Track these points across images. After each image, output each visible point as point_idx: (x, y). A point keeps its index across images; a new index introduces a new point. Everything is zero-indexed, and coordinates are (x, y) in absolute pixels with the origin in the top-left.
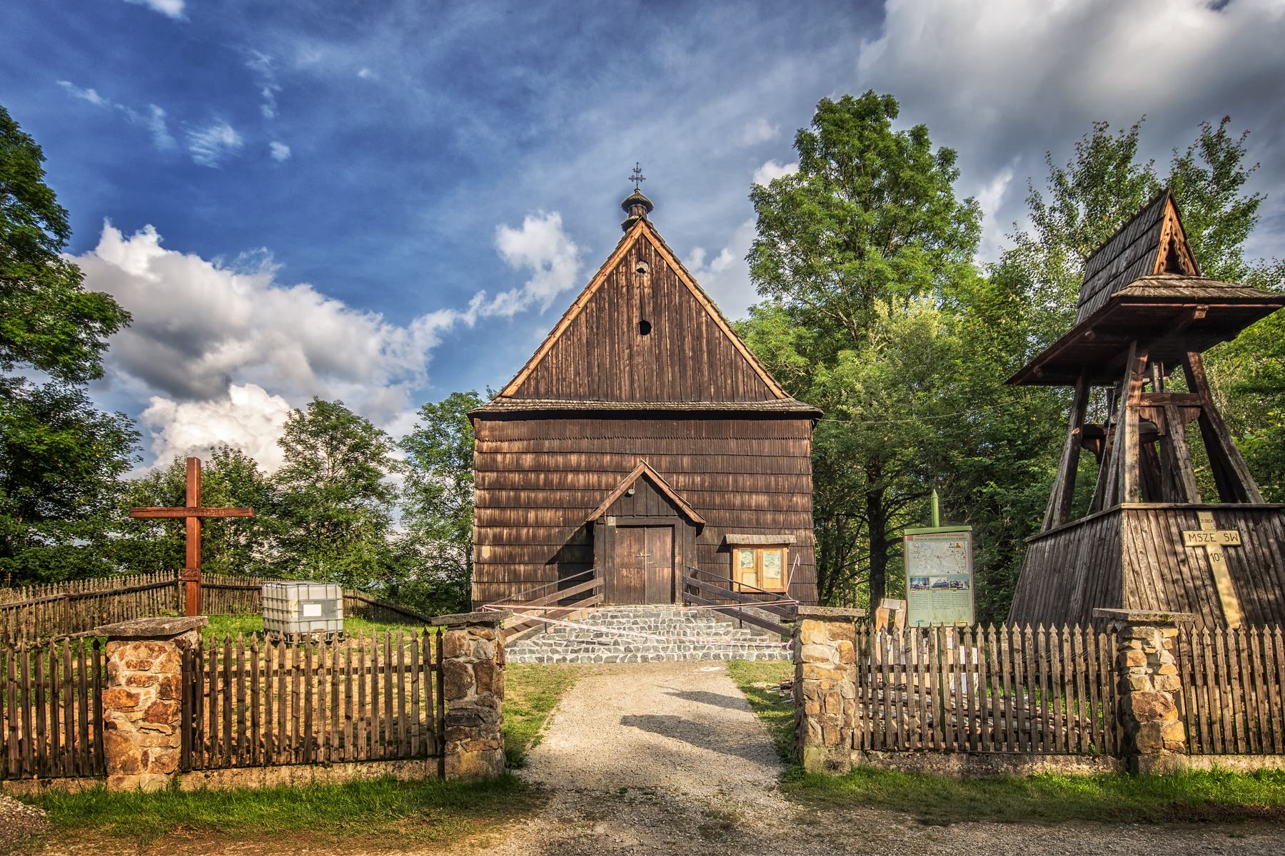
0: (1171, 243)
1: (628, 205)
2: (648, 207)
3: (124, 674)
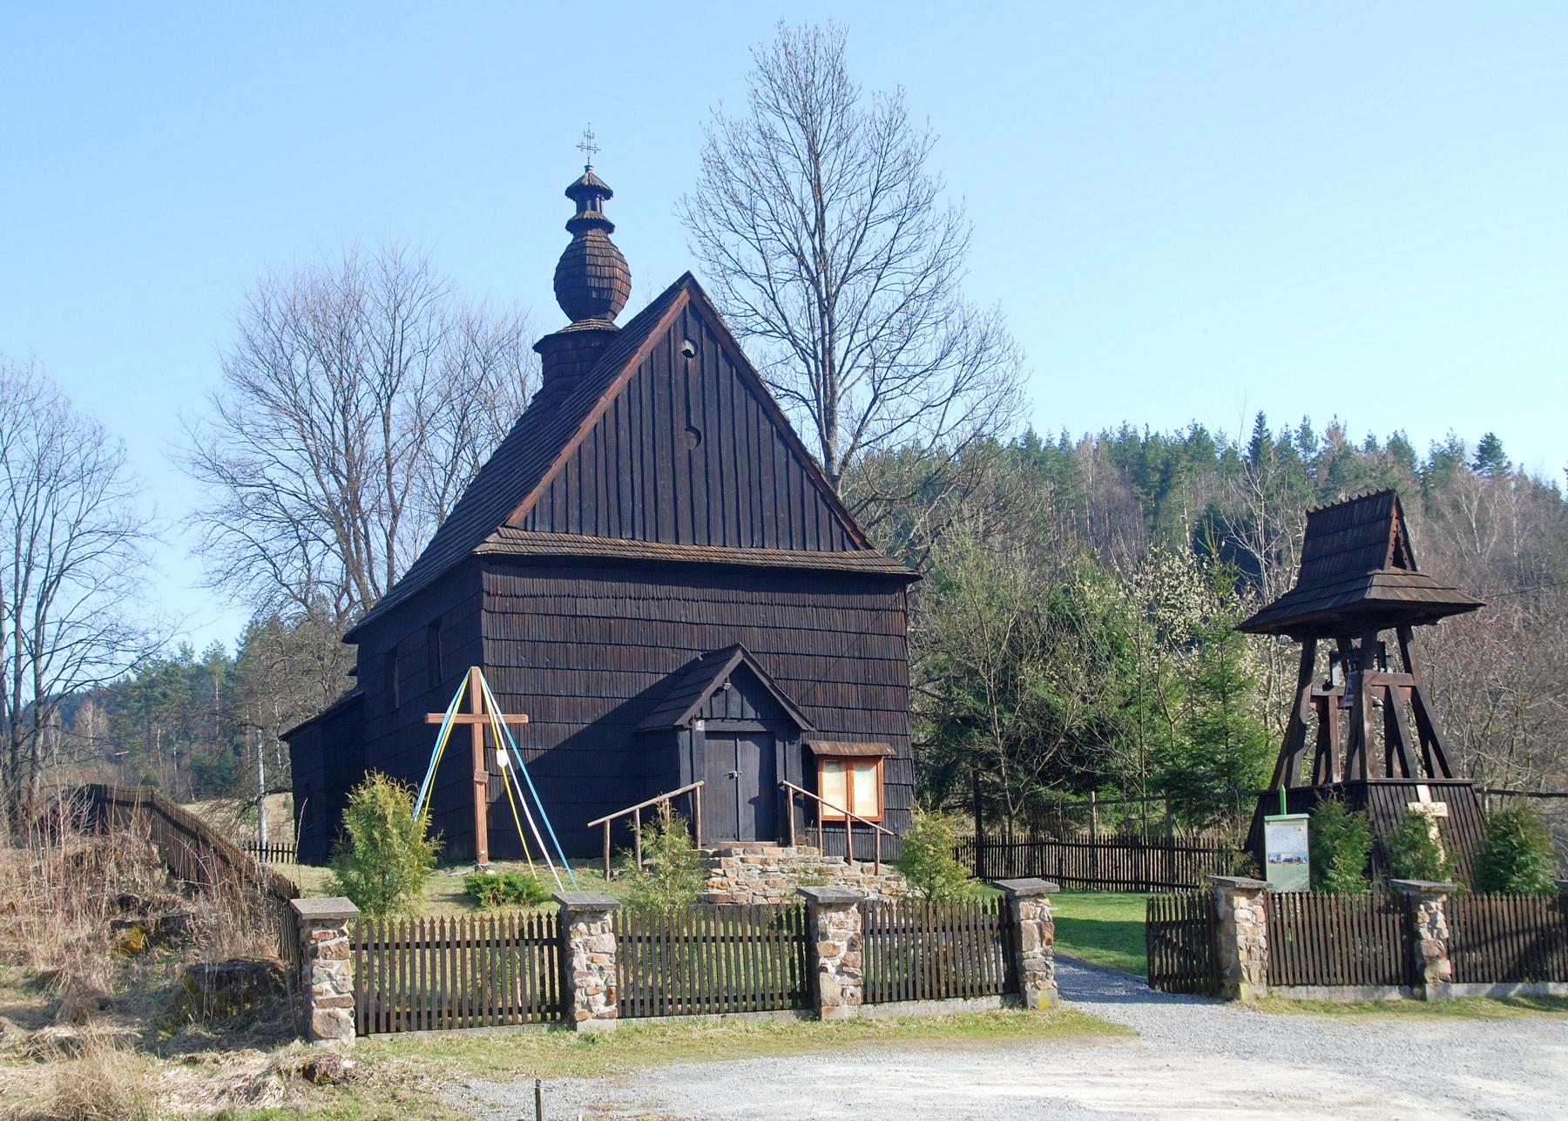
0: (1397, 539)
2: (608, 194)
3: (831, 930)
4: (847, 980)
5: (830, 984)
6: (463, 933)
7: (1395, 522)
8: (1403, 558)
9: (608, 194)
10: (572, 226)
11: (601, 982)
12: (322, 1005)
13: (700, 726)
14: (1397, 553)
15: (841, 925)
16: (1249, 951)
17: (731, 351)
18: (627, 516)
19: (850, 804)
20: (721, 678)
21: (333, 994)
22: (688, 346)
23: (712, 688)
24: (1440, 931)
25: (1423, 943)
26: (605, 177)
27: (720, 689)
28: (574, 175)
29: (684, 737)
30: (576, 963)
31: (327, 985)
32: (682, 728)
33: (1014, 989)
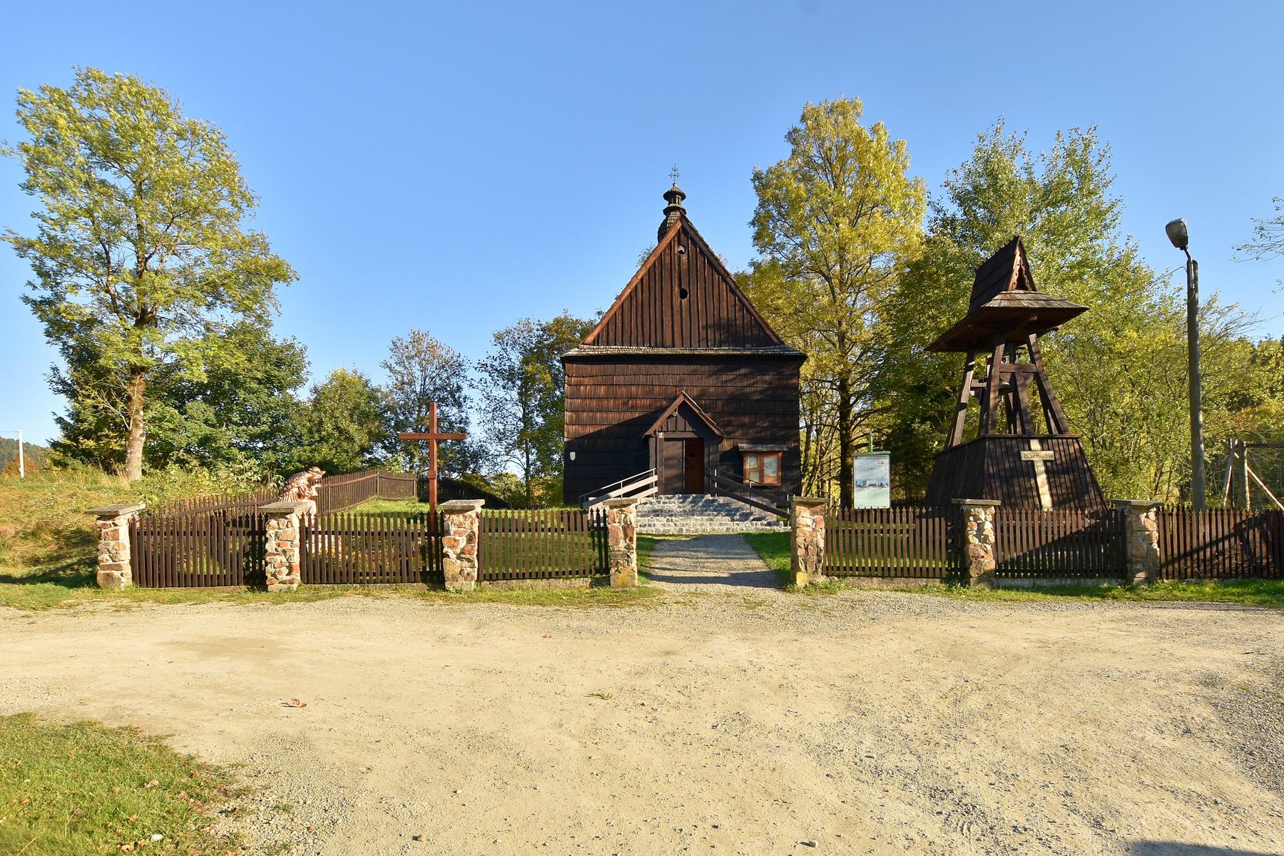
0: (1020, 270)
1: (670, 196)
3: (453, 529)
4: (465, 563)
5: (452, 565)
6: (1087, 564)
7: (1018, 259)
8: (1025, 283)
9: (683, 197)
10: (667, 211)
11: (284, 560)
12: (103, 568)
13: (661, 435)
14: (1020, 279)
15: (460, 525)
16: (806, 549)
17: (704, 249)
18: (647, 336)
19: (863, 485)
20: (673, 409)
21: (110, 562)
22: (682, 248)
23: (666, 414)
24: (987, 537)
25: (971, 546)
26: (680, 187)
27: (671, 416)
28: (669, 188)
29: (652, 441)
30: (267, 546)
31: (106, 556)
32: (650, 436)
33: (601, 573)
